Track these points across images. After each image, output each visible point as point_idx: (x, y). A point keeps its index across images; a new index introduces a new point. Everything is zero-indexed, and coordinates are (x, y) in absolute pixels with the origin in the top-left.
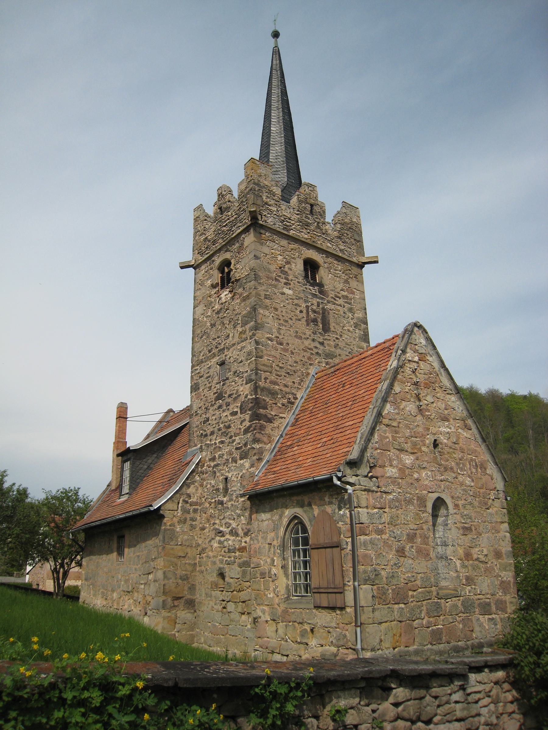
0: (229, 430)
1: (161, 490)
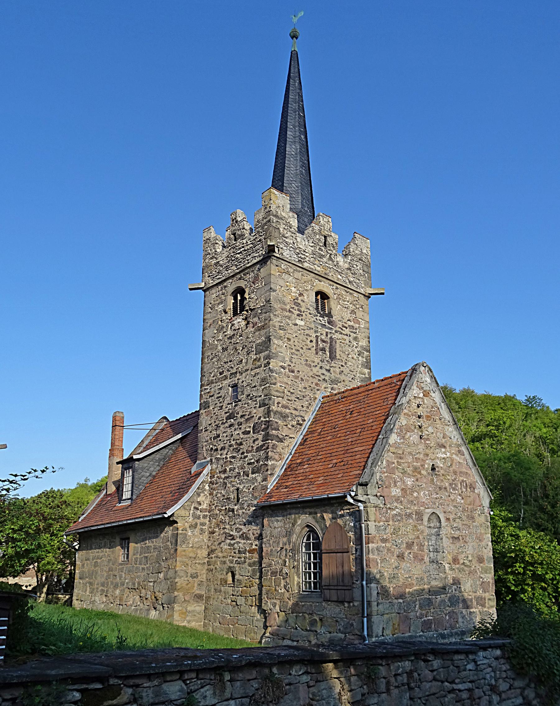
0: (241, 447)
1: (170, 498)
